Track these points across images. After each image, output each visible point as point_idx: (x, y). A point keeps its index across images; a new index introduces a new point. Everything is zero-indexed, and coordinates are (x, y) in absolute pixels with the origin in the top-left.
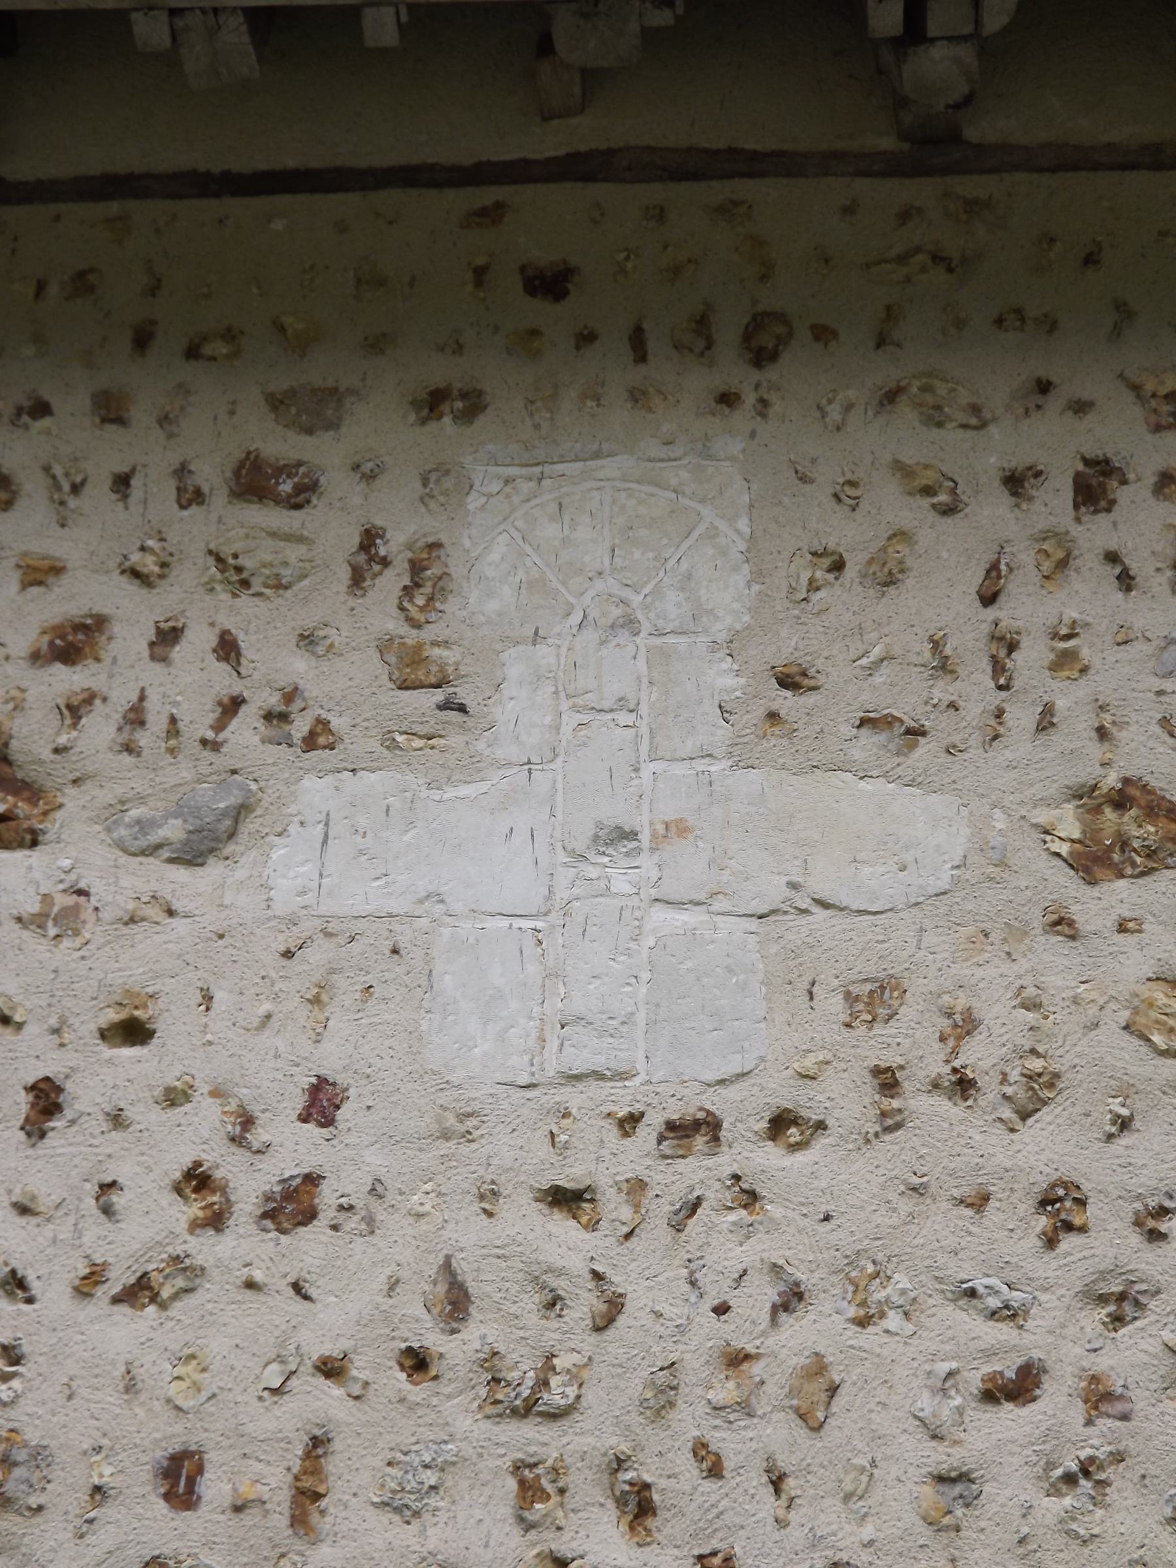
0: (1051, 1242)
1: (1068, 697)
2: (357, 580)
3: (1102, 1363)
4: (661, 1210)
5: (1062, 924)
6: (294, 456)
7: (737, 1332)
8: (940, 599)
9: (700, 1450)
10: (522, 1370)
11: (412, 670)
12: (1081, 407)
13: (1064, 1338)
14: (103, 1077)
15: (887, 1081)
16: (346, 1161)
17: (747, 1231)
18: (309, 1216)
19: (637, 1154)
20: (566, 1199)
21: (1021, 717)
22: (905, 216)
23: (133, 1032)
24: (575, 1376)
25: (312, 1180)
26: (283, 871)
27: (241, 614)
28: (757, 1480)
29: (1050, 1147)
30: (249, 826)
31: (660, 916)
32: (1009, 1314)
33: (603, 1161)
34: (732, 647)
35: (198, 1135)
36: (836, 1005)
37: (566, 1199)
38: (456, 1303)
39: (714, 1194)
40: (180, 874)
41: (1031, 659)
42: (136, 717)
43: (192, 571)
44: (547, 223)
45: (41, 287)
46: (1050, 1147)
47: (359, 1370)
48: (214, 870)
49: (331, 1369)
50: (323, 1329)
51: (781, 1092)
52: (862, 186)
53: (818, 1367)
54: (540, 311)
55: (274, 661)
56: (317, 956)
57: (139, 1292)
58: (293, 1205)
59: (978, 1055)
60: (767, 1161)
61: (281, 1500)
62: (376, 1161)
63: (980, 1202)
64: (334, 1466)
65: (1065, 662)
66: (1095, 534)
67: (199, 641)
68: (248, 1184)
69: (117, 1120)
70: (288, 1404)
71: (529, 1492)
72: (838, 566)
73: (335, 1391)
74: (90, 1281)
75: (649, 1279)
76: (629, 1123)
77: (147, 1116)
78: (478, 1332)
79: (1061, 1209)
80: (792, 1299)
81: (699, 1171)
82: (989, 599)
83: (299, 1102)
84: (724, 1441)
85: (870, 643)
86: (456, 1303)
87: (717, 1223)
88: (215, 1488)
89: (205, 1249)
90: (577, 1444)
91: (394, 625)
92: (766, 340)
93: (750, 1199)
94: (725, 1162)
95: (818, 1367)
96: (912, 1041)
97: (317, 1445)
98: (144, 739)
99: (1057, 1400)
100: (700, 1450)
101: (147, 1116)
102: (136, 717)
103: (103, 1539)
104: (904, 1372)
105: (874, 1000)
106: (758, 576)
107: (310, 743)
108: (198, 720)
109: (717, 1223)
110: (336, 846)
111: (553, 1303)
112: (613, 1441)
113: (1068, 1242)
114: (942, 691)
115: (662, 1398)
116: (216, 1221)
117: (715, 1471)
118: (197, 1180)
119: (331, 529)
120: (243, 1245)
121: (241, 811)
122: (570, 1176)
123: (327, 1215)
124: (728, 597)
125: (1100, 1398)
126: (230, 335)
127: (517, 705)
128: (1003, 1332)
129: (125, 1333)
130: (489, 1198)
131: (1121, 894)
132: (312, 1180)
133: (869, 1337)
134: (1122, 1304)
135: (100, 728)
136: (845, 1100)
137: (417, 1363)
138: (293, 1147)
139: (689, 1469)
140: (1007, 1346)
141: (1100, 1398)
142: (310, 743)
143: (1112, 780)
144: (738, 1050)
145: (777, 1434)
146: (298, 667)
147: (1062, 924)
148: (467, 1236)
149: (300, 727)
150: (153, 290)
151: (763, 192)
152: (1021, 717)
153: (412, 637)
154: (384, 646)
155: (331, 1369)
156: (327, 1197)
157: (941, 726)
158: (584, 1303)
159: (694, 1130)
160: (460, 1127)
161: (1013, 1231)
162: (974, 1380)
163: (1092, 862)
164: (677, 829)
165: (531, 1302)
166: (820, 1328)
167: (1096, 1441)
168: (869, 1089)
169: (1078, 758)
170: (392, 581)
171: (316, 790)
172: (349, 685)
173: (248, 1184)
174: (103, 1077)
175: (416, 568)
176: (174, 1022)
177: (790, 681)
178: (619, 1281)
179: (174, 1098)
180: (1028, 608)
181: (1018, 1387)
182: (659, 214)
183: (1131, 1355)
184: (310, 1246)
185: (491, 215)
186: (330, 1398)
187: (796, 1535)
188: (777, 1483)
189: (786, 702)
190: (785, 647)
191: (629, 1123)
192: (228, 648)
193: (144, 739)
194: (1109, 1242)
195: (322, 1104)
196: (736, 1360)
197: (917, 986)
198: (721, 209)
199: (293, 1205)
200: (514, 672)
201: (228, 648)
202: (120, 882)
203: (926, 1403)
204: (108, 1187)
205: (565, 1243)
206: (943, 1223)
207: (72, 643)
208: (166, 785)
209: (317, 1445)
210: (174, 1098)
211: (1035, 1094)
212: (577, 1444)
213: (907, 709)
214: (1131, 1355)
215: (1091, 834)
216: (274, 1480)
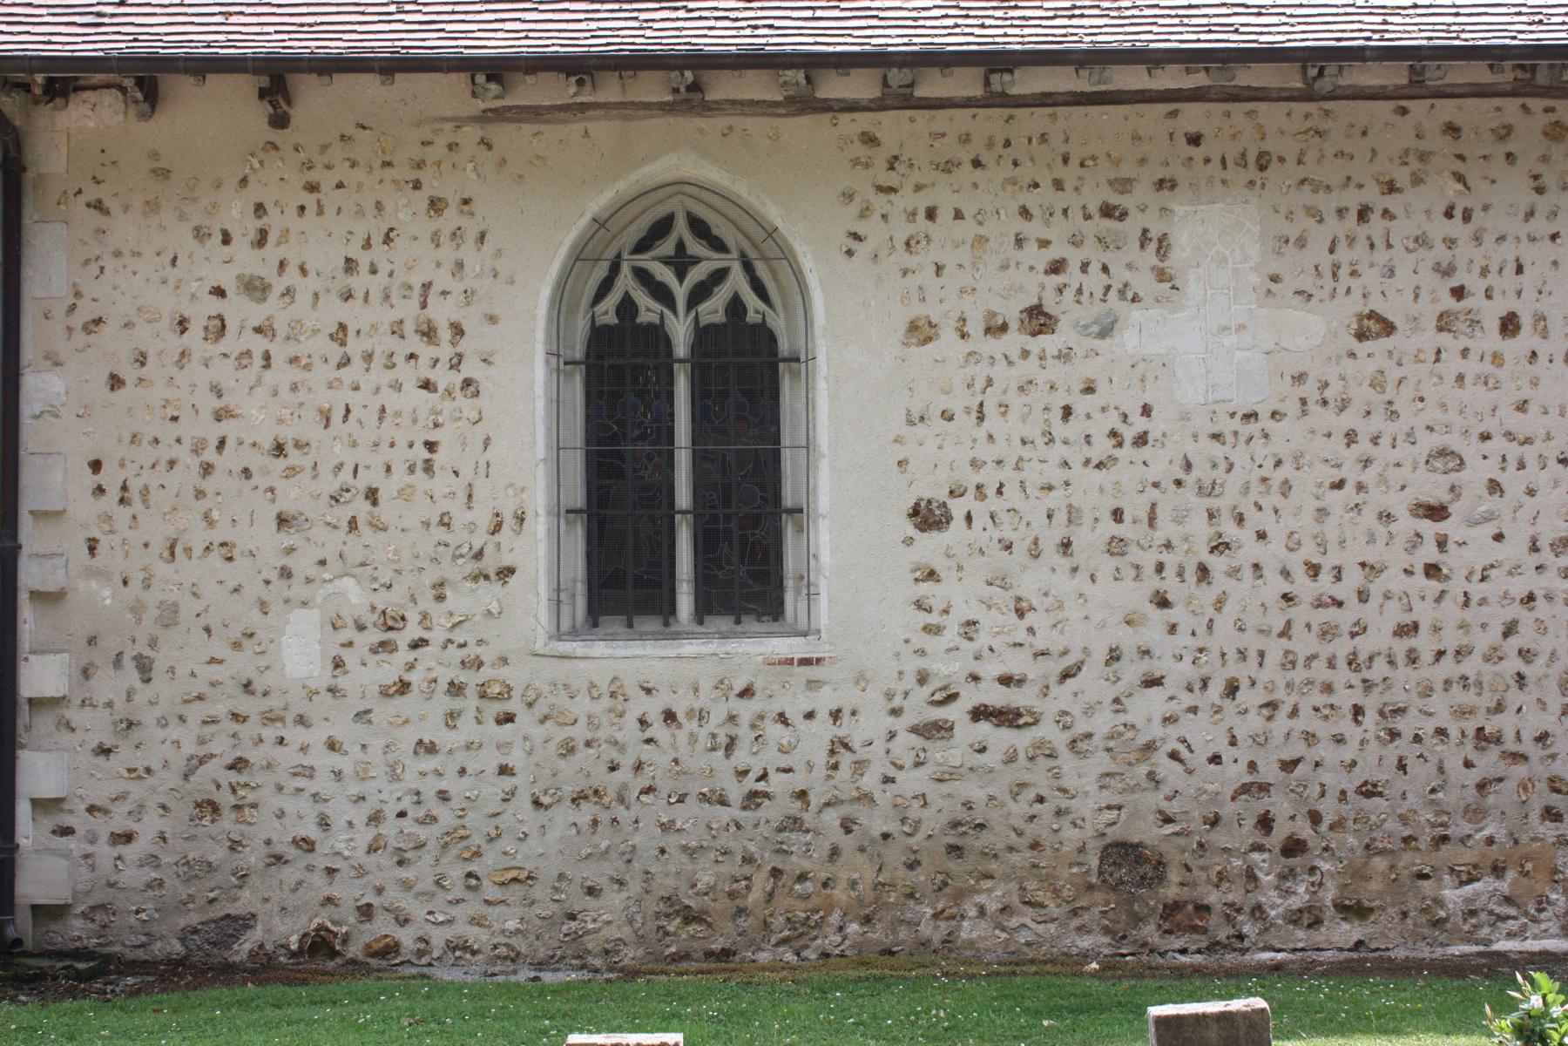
0: (1348, 445)
1: (1355, 284)
2: (1142, 246)
3: (1361, 479)
4: (1242, 439)
5: (1352, 355)
6: (1117, 203)
7: (1264, 473)
8: (1317, 253)
9: (1256, 504)
10: (1207, 482)
11: (1162, 276)
12: (1361, 186)
13: (1351, 473)
14: (1081, 404)
15: (1304, 402)
16: (1155, 426)
17: (1266, 445)
18: (1145, 443)
19: (1236, 423)
20: (1216, 437)
21: (1341, 290)
22: (1307, 116)
23: (1089, 390)
24: (1222, 486)
25: (1146, 433)
26: (1129, 340)
27: (1108, 257)
28: (1271, 512)
29: (1349, 419)
30: (1117, 326)
31: (1238, 354)
32: (1338, 466)
33: (1227, 426)
34: (1256, 269)
35: (1113, 421)
36: (1288, 379)
37: (1216, 437)
38: (1188, 466)
39: (1257, 434)
40: (1098, 342)
41: (1344, 272)
42: (1080, 291)
43: (1090, 241)
44: (1193, 116)
45: (1030, 141)
46: (1349, 419)
47: (1163, 485)
48: (1108, 340)
49: (1156, 485)
50: (1154, 473)
51: (1276, 406)
52: (1293, 104)
53: (1286, 482)
54: (1192, 151)
55: (1119, 275)
56: (1141, 366)
57: (1100, 465)
58: (1141, 440)
59: (1329, 394)
60: (1271, 425)
61: (1146, 520)
62: (1163, 427)
63: (1329, 435)
64: (1158, 511)
65: (1354, 273)
66: (1362, 231)
67: (1095, 268)
68: (1128, 434)
69: (1088, 416)
70: (1144, 495)
71: (1211, 516)
72: (1287, 241)
73: (1156, 491)
74: (1087, 462)
75: (1240, 456)
76: (1233, 415)
77: (1097, 415)
78: (1195, 473)
79: (1351, 437)
80: (1278, 463)
81: (1252, 428)
82: (1331, 251)
83: (1140, 410)
84: (1262, 502)
85: (1297, 268)
86: (1188, 466)
87: (1258, 442)
88: (1127, 517)
89: (1117, 452)
90: (1222, 504)
91: (1155, 261)
92: (1263, 162)
93: (1266, 436)
94: (1259, 425)
95: (1286, 482)
96: (1310, 390)
97: (1153, 505)
98: (1083, 299)
99: (1349, 488)
100: (1256, 504)
101: (1097, 415)
102: (1080, 291)
103: (1099, 531)
104: (1309, 482)
105: (1300, 378)
106: (1263, 244)
107: (1133, 300)
108: (1099, 293)
109: (1258, 442)
110: (1144, 332)
111: (1214, 466)
112: (836, 892)
113: (1353, 446)
114: (1320, 283)
115: (1246, 489)
116: (1120, 445)
117: (1260, 509)
118: (1113, 434)
119: (1131, 228)
120: (1127, 451)
121: (1113, 323)
122: (1215, 430)
123: (1151, 442)
124: (1254, 251)
125: (1360, 487)
126: (1093, 158)
127: (1193, 287)
128: (1335, 471)
129: (1099, 476)
130: (1195, 437)
131: (1369, 345)
132: (1146, 433)
133: (1299, 473)
134: (1367, 463)
135: (1069, 294)
136: (1292, 407)
137: (1178, 483)
138: (1139, 424)
139: (1253, 509)
140: (1336, 475)
141: (1360, 487)
142: (1133, 300)
143: (1366, 311)
144: (1260, 397)
145: (1275, 499)
146: (1127, 276)
147: (1352, 355)
148: (1191, 449)
149: (1130, 295)
150: (1067, 141)
151: (1262, 107)
152: (1341, 290)
153: (1161, 265)
154: (1153, 269)
155: (1156, 485)
156: (1151, 438)
157: (1318, 294)
158: (1223, 466)
159: (1250, 416)
160: (1185, 417)
161: (1338, 441)
162: (1327, 484)
163: (1361, 336)
164: (1242, 327)
165: (1209, 465)
166: (1286, 471)
167: (1359, 499)
168: (1298, 404)
169: (1356, 305)
170: (1153, 246)
171: (1136, 314)
172: (1143, 282)
173: (1128, 434)
174: (1081, 404)
175: (1160, 241)
176: (1102, 387)
177: (1275, 279)
178: (1232, 459)
179: (1103, 409)
180: (1344, 255)
181: (1339, 485)
182: (1228, 115)
183: (1369, 476)
184: (1146, 452)
185: (1173, 114)
186: (1153, 494)
187: (1282, 525)
188: (1276, 512)
189: (1273, 286)
190: (1274, 267)
191: (1233, 415)
192: (1105, 269)
193: (1083, 299)
194: (1363, 447)
195: (1146, 411)
196: (1264, 480)
197: (1312, 374)
198: (1243, 155)
199: (1141, 440)
200: (1192, 277)
201: (1105, 269)
202: (1082, 345)
203: (1315, 490)
204: (1088, 436)
205: (1218, 451)
206: (1320, 441)
207: (1056, 267)
208: (1091, 311)
209: (1153, 505)
210: (1103, 409)
211: (1344, 405)
212: (1222, 504)
213: (1309, 288)
214: (1369, 476)
215: (1361, 327)
216: (1143, 515)
